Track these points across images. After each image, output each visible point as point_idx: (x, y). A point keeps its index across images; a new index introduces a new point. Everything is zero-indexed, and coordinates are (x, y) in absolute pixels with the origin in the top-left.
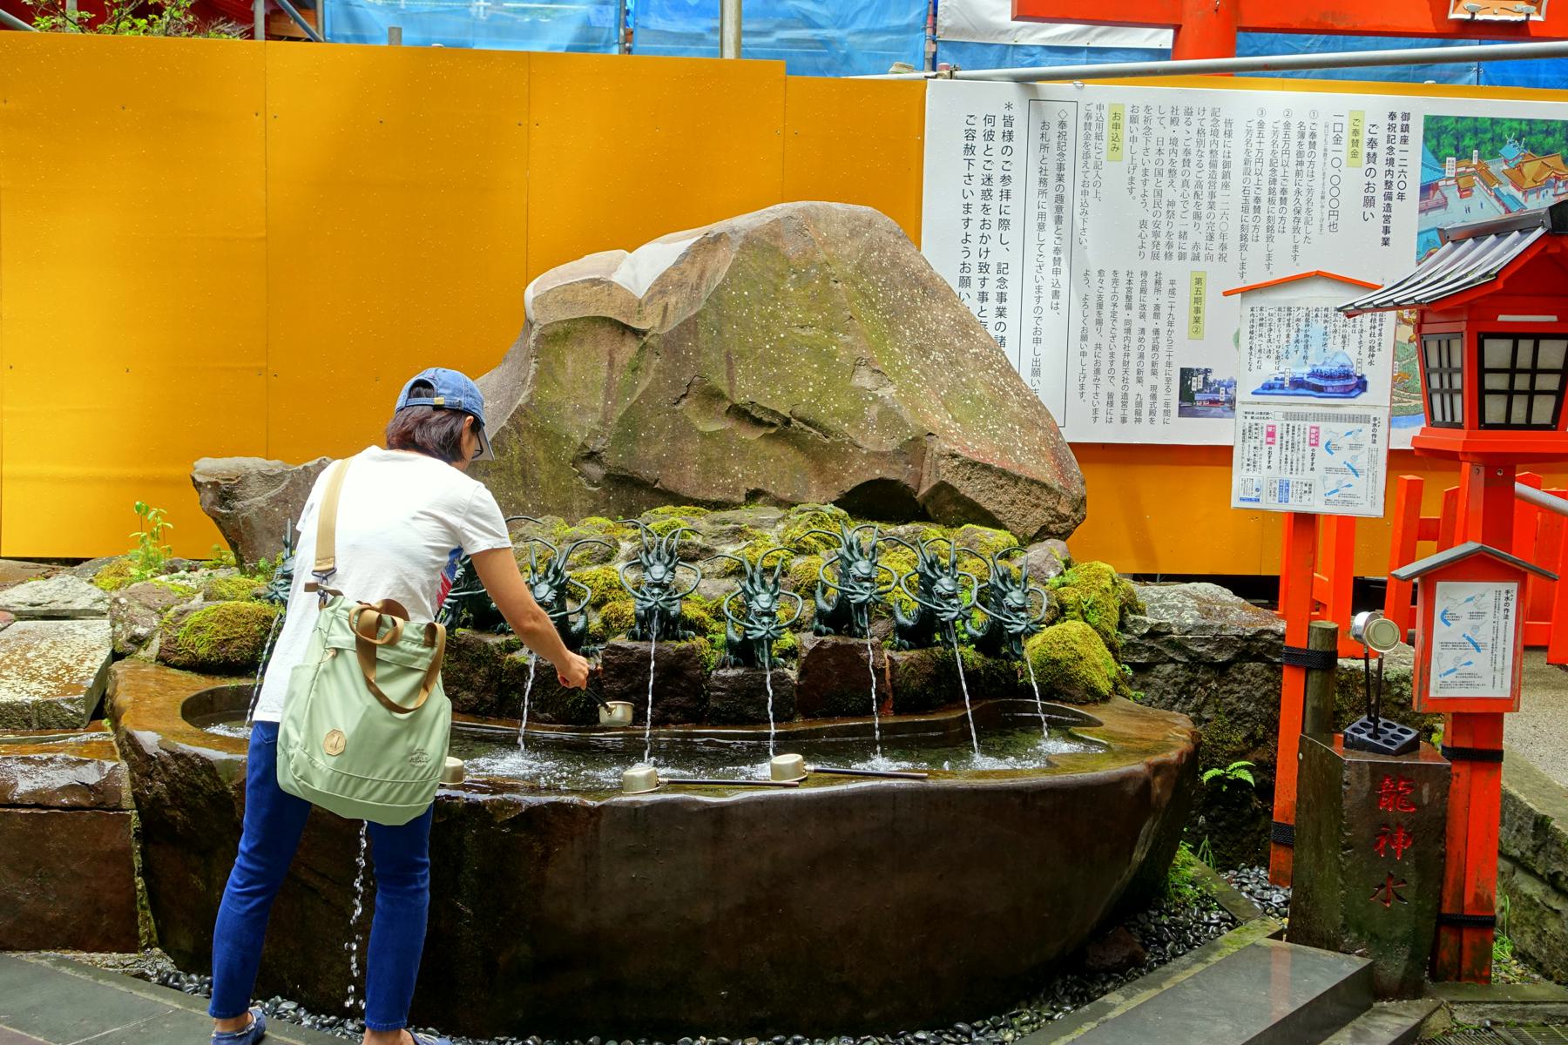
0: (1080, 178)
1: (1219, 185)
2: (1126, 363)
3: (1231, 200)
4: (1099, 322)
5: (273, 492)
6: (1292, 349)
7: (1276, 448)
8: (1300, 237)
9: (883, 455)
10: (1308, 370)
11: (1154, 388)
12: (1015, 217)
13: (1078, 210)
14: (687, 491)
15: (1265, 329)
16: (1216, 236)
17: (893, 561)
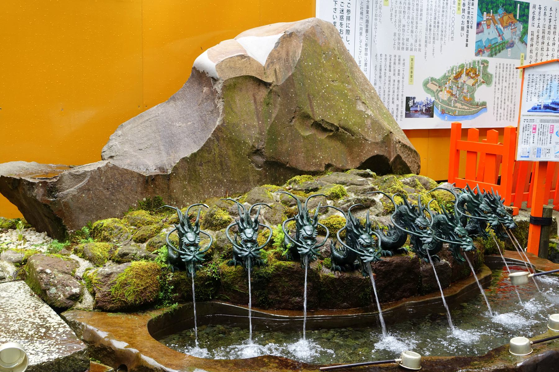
0: (374, 13)
1: (419, 19)
2: (389, 95)
3: (422, 25)
4: (380, 77)
5: (80, 185)
6: (544, 92)
7: (536, 134)
8: (443, 42)
9: (377, 143)
10: (550, 101)
11: (398, 105)
12: (352, 30)
13: (374, 27)
14: (300, 167)
15: (534, 84)
16: (418, 41)
17: (386, 195)
